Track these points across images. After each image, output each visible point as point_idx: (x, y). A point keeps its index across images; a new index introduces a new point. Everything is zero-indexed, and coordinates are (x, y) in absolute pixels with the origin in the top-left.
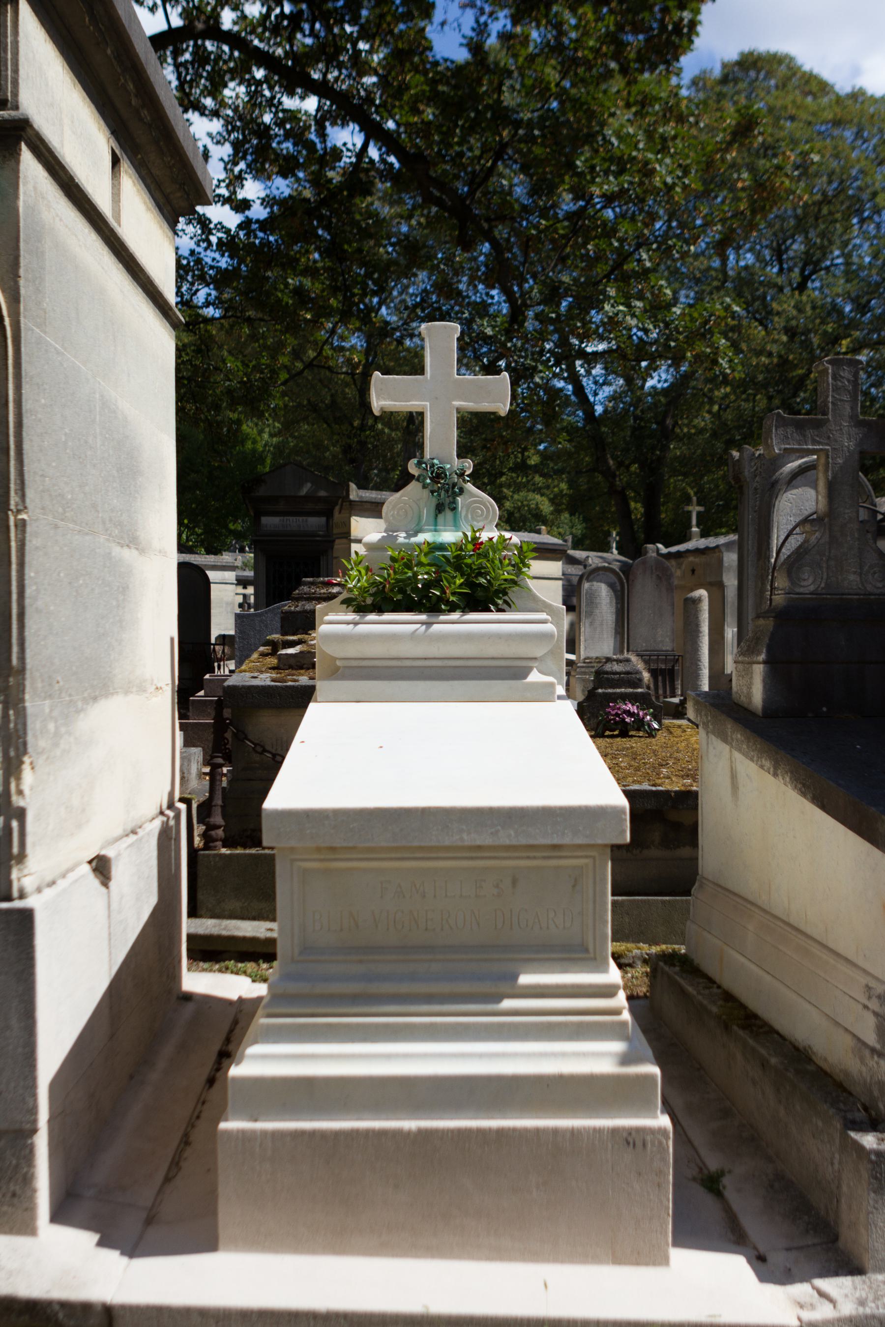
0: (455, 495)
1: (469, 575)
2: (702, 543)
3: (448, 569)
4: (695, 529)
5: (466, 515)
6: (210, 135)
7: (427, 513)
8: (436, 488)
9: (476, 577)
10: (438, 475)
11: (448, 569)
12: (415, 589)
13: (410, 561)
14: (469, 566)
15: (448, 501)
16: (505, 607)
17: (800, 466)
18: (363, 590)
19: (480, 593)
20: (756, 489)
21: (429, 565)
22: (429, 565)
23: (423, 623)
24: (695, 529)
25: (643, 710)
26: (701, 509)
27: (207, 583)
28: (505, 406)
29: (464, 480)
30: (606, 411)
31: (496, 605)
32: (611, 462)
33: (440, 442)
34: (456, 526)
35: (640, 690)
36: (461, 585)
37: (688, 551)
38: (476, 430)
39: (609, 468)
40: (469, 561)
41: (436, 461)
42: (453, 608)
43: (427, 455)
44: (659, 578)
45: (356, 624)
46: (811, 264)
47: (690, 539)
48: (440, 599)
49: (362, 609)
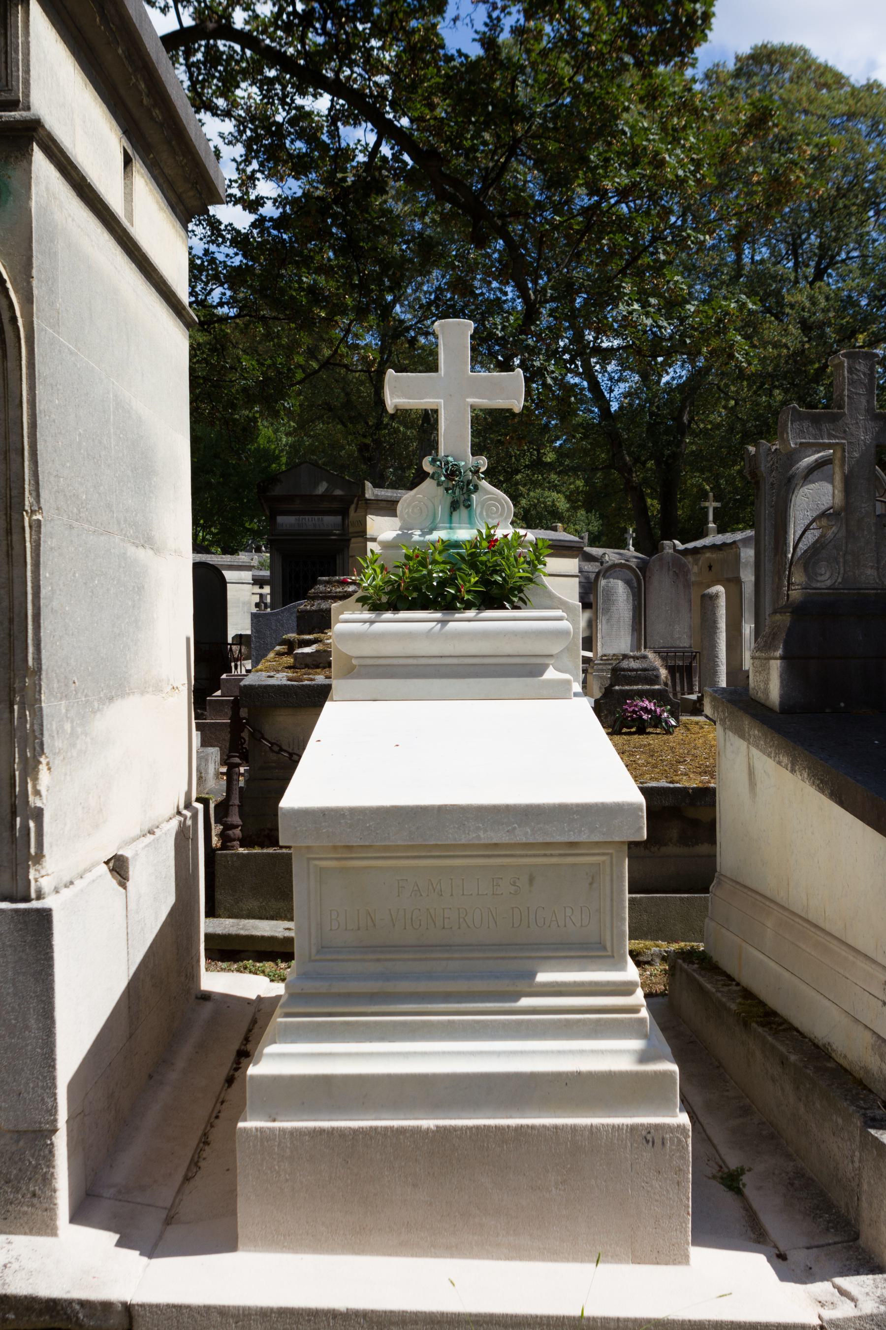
0: (470, 492)
1: (484, 573)
2: (719, 539)
3: (464, 566)
5: (481, 513)
6: (221, 135)
7: (441, 510)
8: (450, 485)
9: (491, 575)
10: (453, 473)
11: (464, 566)
12: (430, 587)
13: (424, 559)
14: (483, 563)
15: (462, 498)
16: (521, 604)
17: (816, 460)
19: (495, 591)
20: (772, 484)
21: (444, 563)
22: (444, 563)
23: (438, 621)
25: (660, 706)
29: (479, 477)
30: (621, 408)
31: (511, 602)
33: (455, 440)
34: (471, 523)
35: (657, 687)
36: (476, 582)
37: (705, 547)
38: (490, 427)
40: (484, 558)
41: (450, 459)
42: (468, 606)
45: (372, 622)
47: (707, 535)
48: (455, 597)
49: (377, 607)
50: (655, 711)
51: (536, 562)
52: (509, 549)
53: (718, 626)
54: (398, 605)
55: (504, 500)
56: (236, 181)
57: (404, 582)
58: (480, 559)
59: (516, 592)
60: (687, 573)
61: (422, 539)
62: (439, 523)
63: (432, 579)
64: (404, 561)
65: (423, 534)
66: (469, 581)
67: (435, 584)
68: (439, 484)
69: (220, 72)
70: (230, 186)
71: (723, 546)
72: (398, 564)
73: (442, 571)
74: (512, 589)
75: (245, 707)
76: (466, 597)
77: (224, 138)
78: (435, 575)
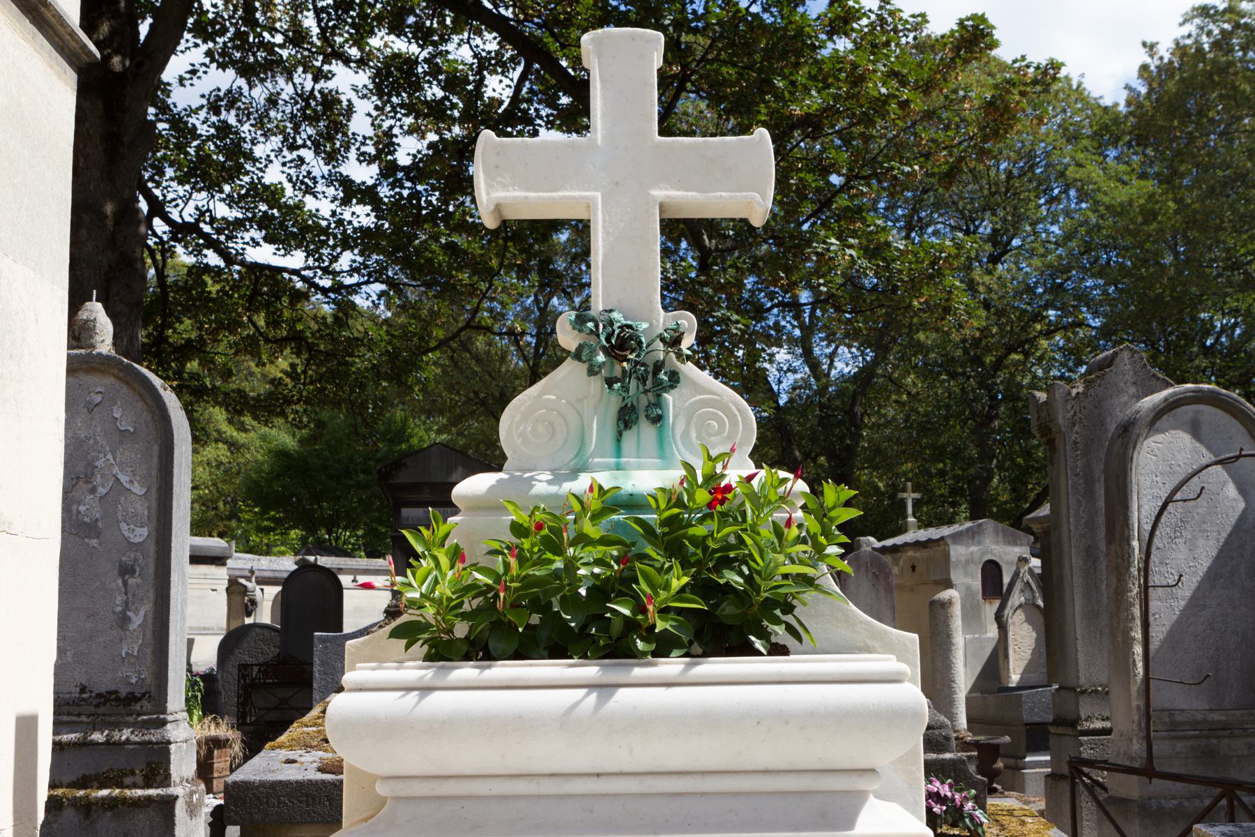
0: (660, 388)
1: (699, 563)
2: (923, 535)
3: (649, 550)
4: (911, 519)
5: (686, 434)
6: (355, 89)
7: (599, 427)
8: (617, 372)
9: (717, 569)
10: (622, 343)
11: (649, 550)
12: (571, 601)
13: (557, 532)
14: (700, 542)
15: (644, 401)
16: (790, 641)
17: (1166, 399)
18: (449, 608)
19: (728, 610)
20: (1075, 443)
21: (604, 541)
22: (604, 541)
23: (591, 686)
24: (911, 519)
25: (961, 790)
26: (917, 495)
27: (339, 589)
28: (764, 198)
29: (679, 355)
30: (791, 401)
31: (764, 635)
32: (798, 453)
33: (626, 279)
34: (663, 452)
35: (948, 756)
36: (682, 590)
37: (906, 544)
38: (701, 253)
39: (796, 459)
40: (700, 531)
41: (615, 315)
42: (664, 646)
43: (598, 305)
44: (875, 576)
45: (426, 690)
46: (999, 248)
47: (906, 531)
48: (630, 626)
49: (442, 651)
50: (953, 800)
51: (822, 539)
52: (758, 506)
53: (954, 641)
54: (491, 645)
55: (736, 405)
56: (371, 138)
57: (507, 588)
58: (691, 531)
59: (778, 612)
60: (888, 575)
61: (554, 489)
62: (593, 455)
63: (576, 582)
64: (510, 538)
65: (557, 479)
66: (667, 586)
67: (583, 591)
68: (592, 371)
69: (352, 17)
70: (363, 144)
71: (928, 543)
72: (496, 546)
73: (598, 562)
74: (770, 604)
75: (234, 824)
76: (660, 626)
77: (357, 92)
78: (582, 572)
